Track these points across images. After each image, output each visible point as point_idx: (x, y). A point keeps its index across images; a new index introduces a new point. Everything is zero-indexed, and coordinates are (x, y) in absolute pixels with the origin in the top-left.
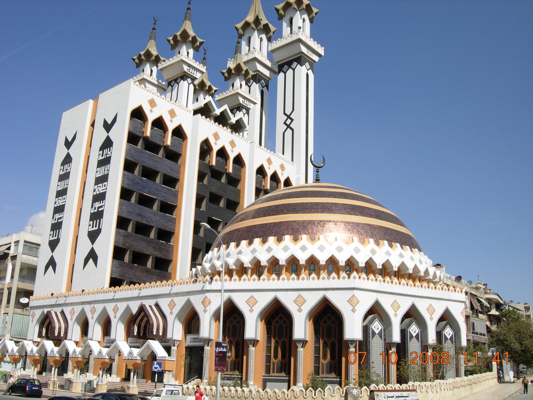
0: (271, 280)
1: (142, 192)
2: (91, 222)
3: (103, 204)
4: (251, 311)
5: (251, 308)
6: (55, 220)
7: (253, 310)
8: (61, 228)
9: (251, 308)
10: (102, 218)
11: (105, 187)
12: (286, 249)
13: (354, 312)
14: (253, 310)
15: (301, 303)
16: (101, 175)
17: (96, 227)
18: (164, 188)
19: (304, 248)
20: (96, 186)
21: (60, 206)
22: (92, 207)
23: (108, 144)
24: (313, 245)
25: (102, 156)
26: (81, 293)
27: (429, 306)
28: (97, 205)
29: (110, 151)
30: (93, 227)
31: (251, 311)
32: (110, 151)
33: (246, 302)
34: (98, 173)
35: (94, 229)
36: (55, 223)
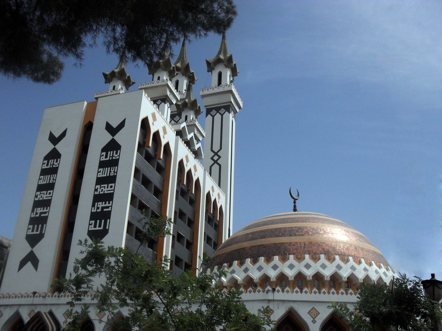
0: (313, 293)
1: (141, 199)
2: (93, 222)
3: (48, 210)
4: (314, 322)
5: (314, 319)
6: (37, 213)
7: (316, 322)
8: (46, 223)
9: (314, 319)
10: (46, 223)
11: (51, 195)
12: (275, 267)
13: (314, 323)
14: (316, 322)
15: (315, 315)
16: (45, 183)
17: (37, 231)
18: (154, 198)
19: (291, 267)
20: (38, 193)
21: (43, 200)
22: (33, 211)
23: (54, 155)
24: (268, 264)
25: (47, 165)
26: (32, 295)
27: (32, 311)
28: (39, 210)
29: (57, 162)
30: (33, 231)
31: (314, 322)
32: (57, 162)
33: (308, 313)
34: (41, 181)
35: (35, 233)
36: (35, 217)
